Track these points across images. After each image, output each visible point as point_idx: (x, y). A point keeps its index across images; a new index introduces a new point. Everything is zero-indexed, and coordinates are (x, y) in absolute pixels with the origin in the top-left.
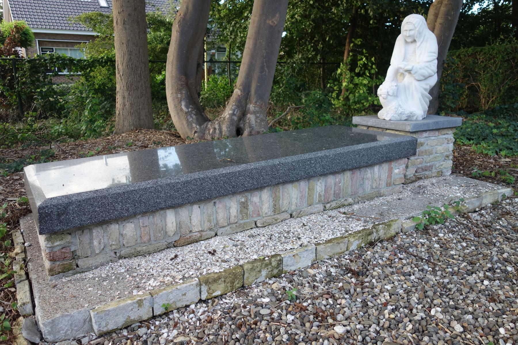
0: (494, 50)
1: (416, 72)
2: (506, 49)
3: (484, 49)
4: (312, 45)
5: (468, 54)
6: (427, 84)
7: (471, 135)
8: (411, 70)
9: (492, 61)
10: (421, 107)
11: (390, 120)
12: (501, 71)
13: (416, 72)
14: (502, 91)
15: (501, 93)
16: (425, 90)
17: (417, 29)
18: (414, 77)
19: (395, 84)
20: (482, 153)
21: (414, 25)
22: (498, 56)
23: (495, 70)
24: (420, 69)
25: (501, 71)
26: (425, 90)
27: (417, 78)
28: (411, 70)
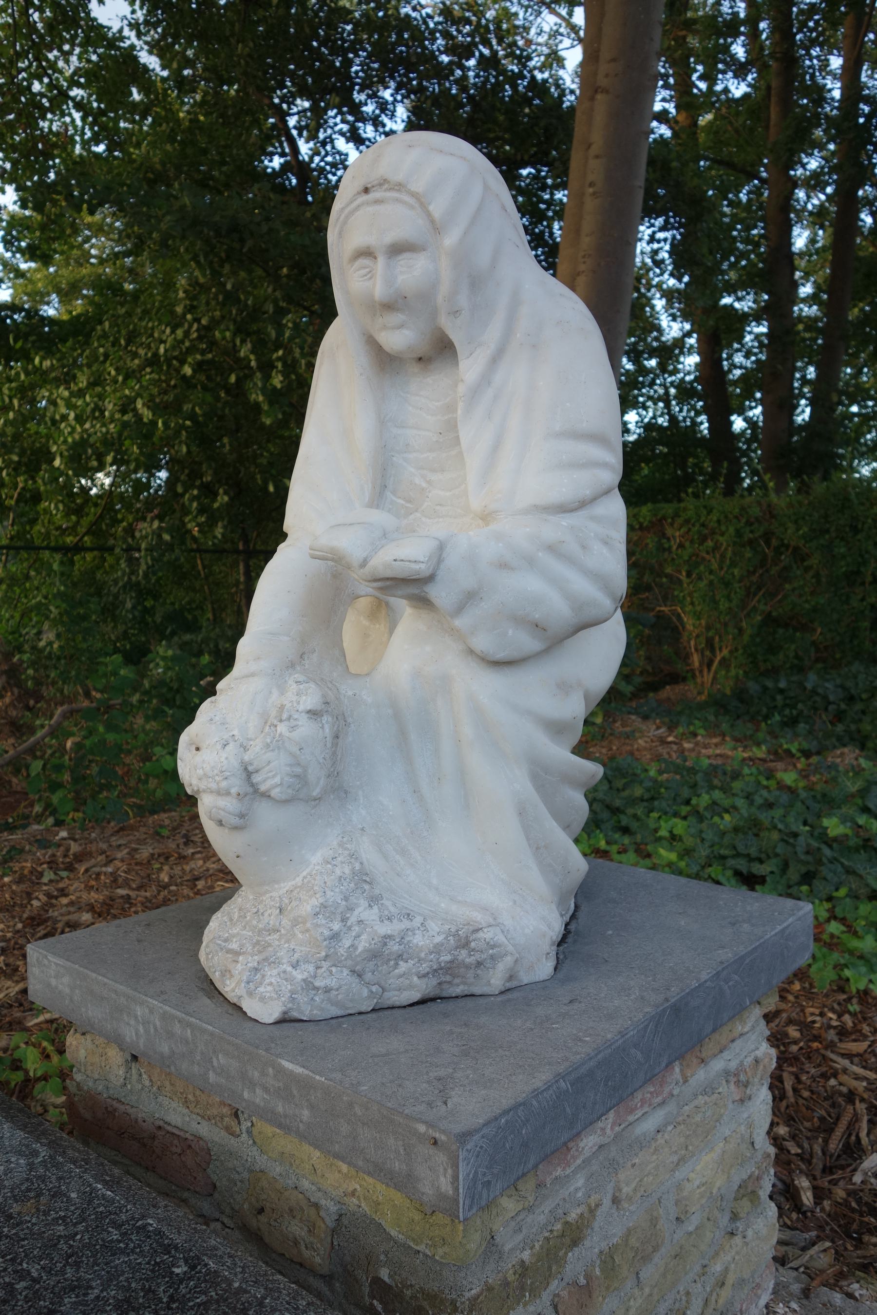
0: (710, 511)
1: (470, 597)
2: (743, 509)
3: (685, 509)
4: (195, 492)
5: (641, 524)
6: (564, 687)
7: (750, 859)
8: (430, 579)
9: (710, 543)
10: (535, 877)
11: (284, 1020)
12: (736, 571)
13: (470, 597)
14: (749, 631)
15: (746, 638)
16: (555, 728)
17: (450, 240)
18: (456, 634)
19: (311, 700)
20: (842, 985)
21: (421, 202)
22: (723, 528)
23: (721, 568)
24: (503, 566)
25: (736, 571)
26: (555, 728)
27: (482, 642)
28: (430, 579)
